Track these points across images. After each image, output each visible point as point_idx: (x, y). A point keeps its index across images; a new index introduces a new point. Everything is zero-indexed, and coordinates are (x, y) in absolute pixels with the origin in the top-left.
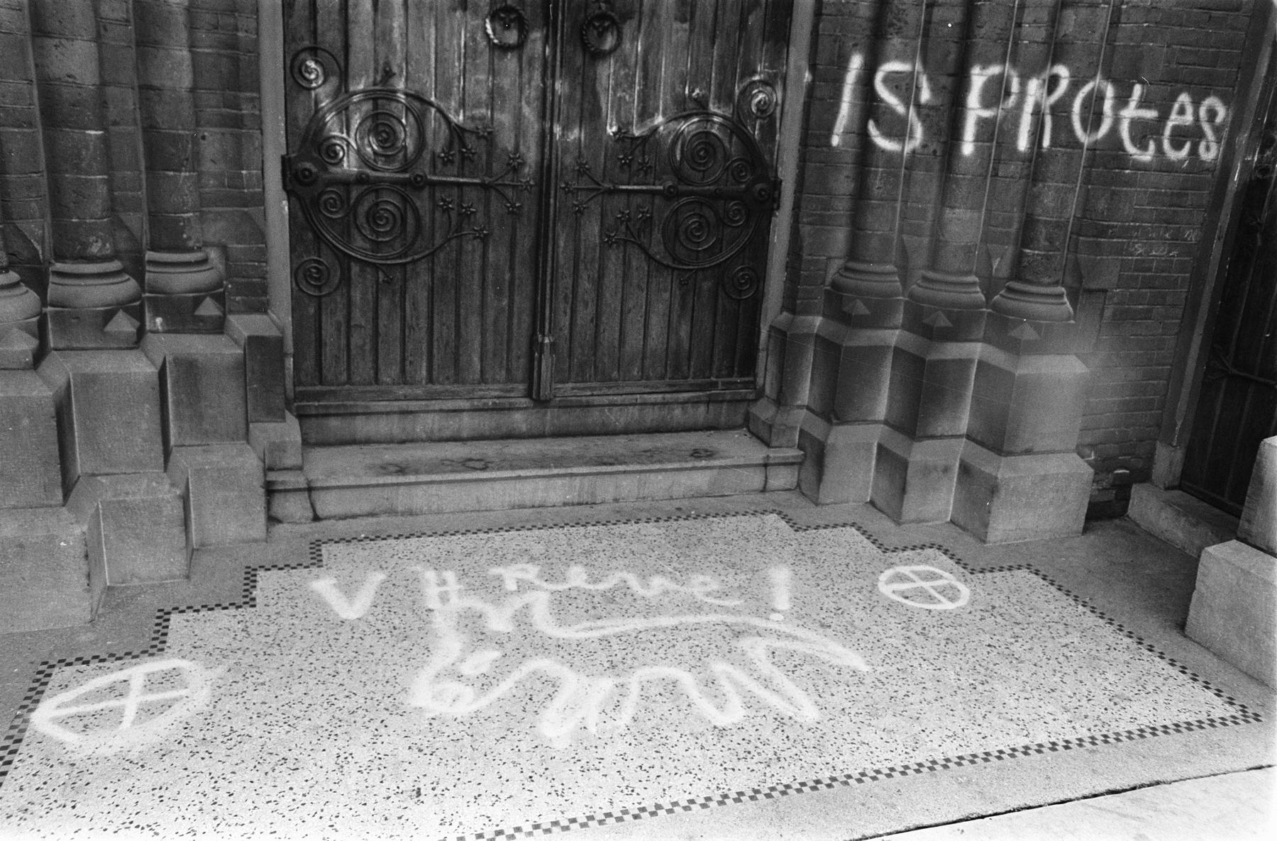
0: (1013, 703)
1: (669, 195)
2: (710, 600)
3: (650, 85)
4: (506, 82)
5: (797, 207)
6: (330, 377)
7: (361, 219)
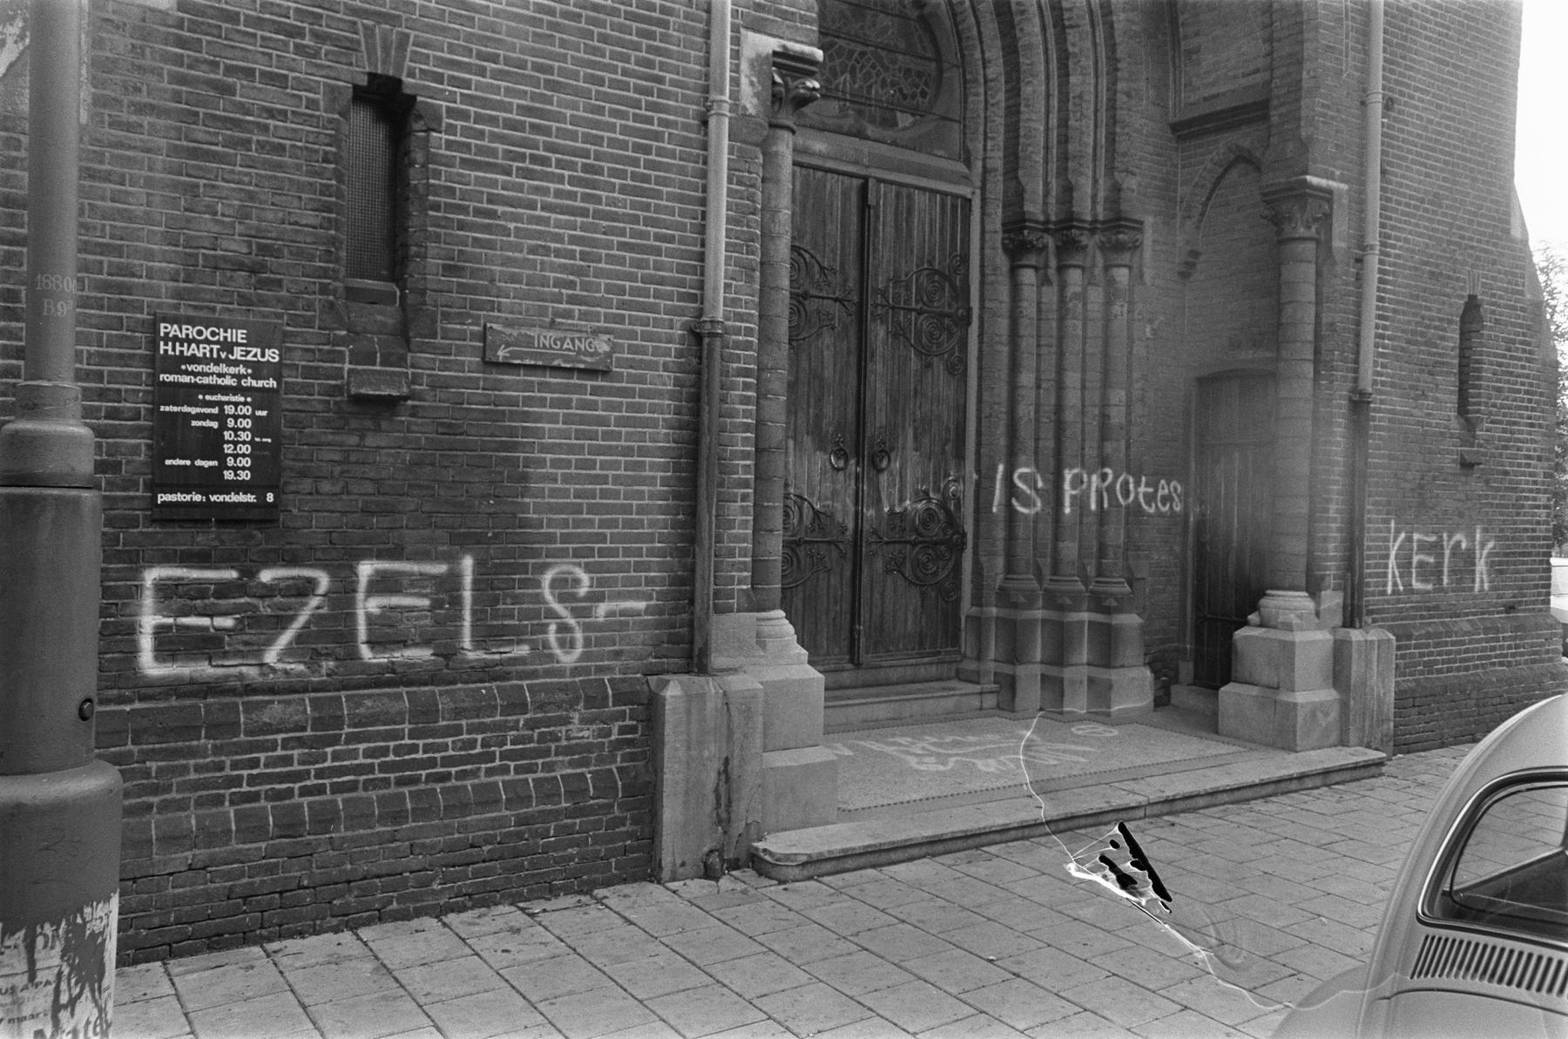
5: (976, 547)
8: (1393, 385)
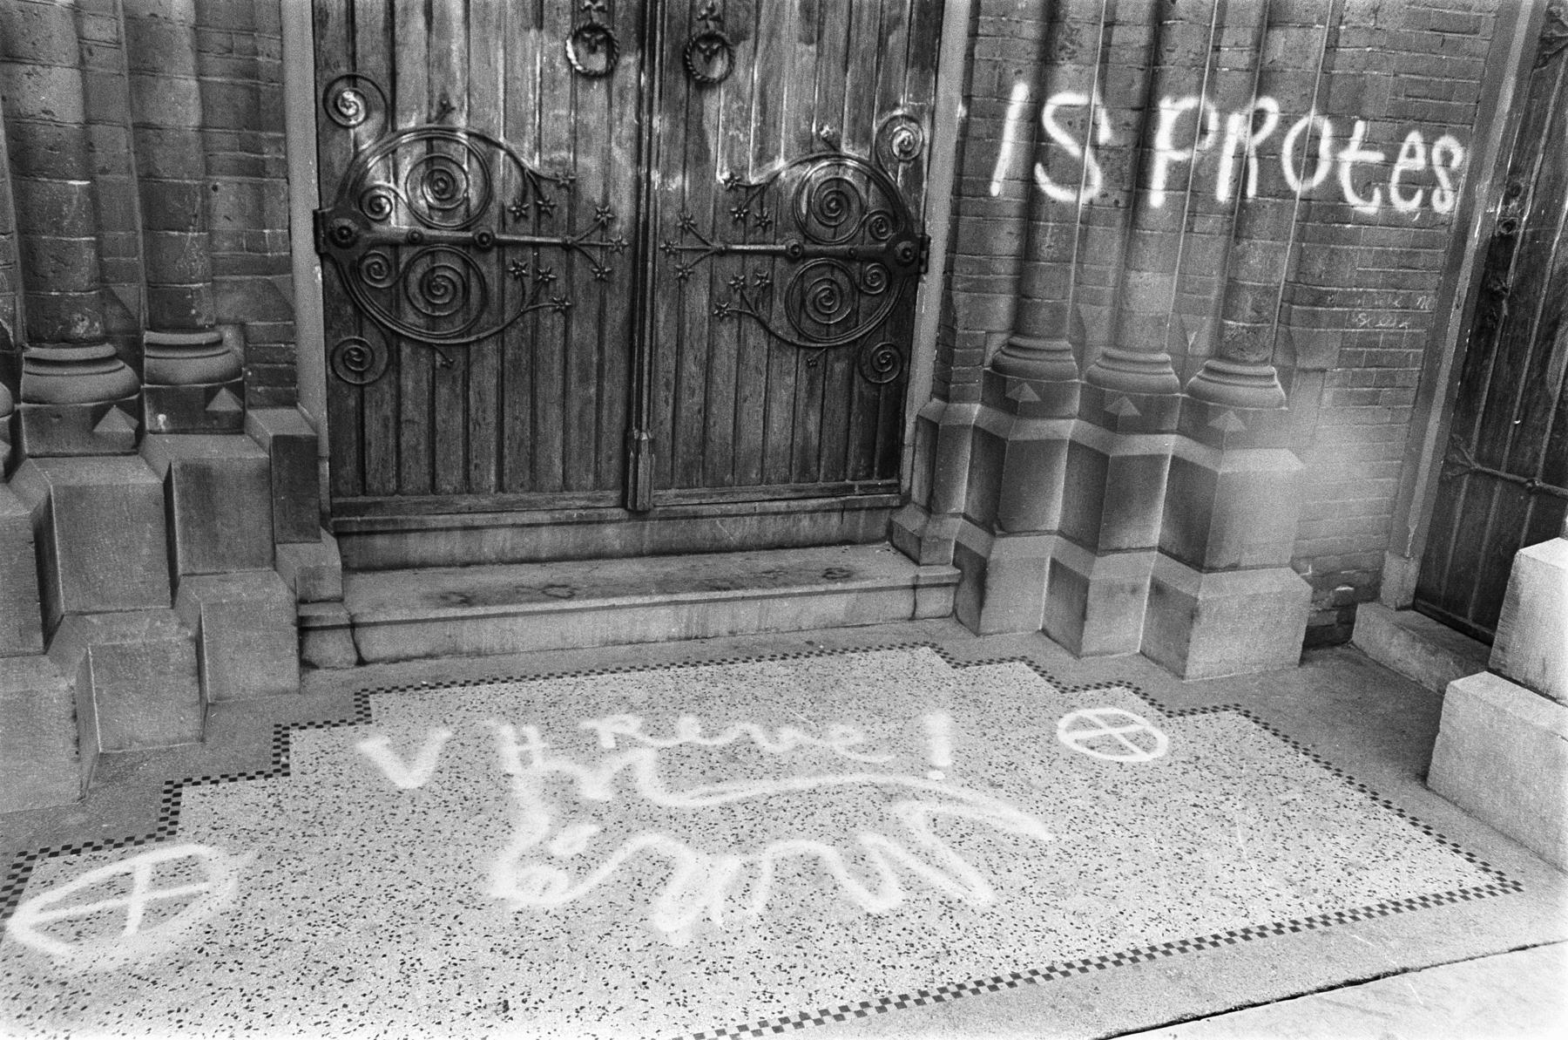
0: (1226, 876)
1: (793, 257)
2: (854, 756)
3: (770, 120)
4: (592, 118)
5: (949, 270)
6: (376, 486)
7: (414, 289)
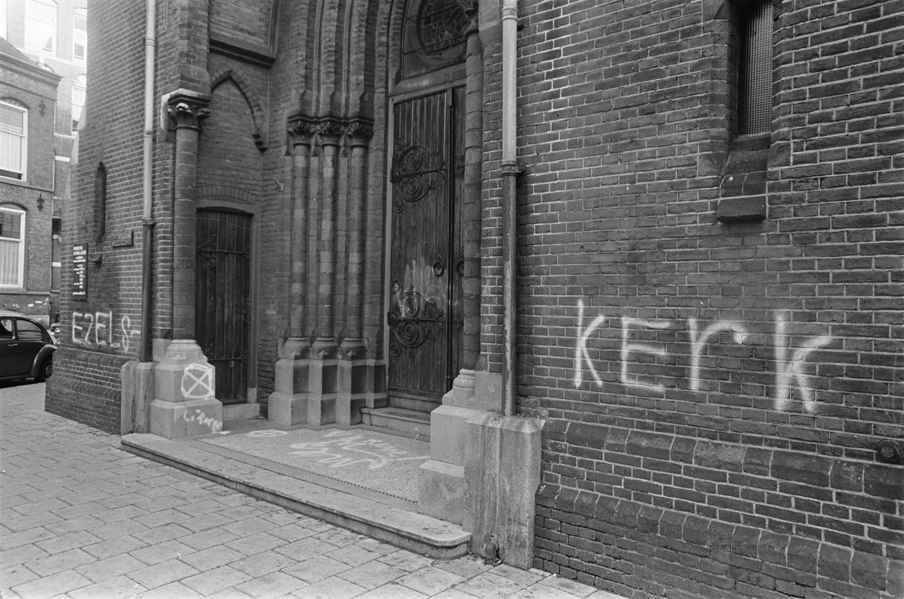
8: (572, 145)
